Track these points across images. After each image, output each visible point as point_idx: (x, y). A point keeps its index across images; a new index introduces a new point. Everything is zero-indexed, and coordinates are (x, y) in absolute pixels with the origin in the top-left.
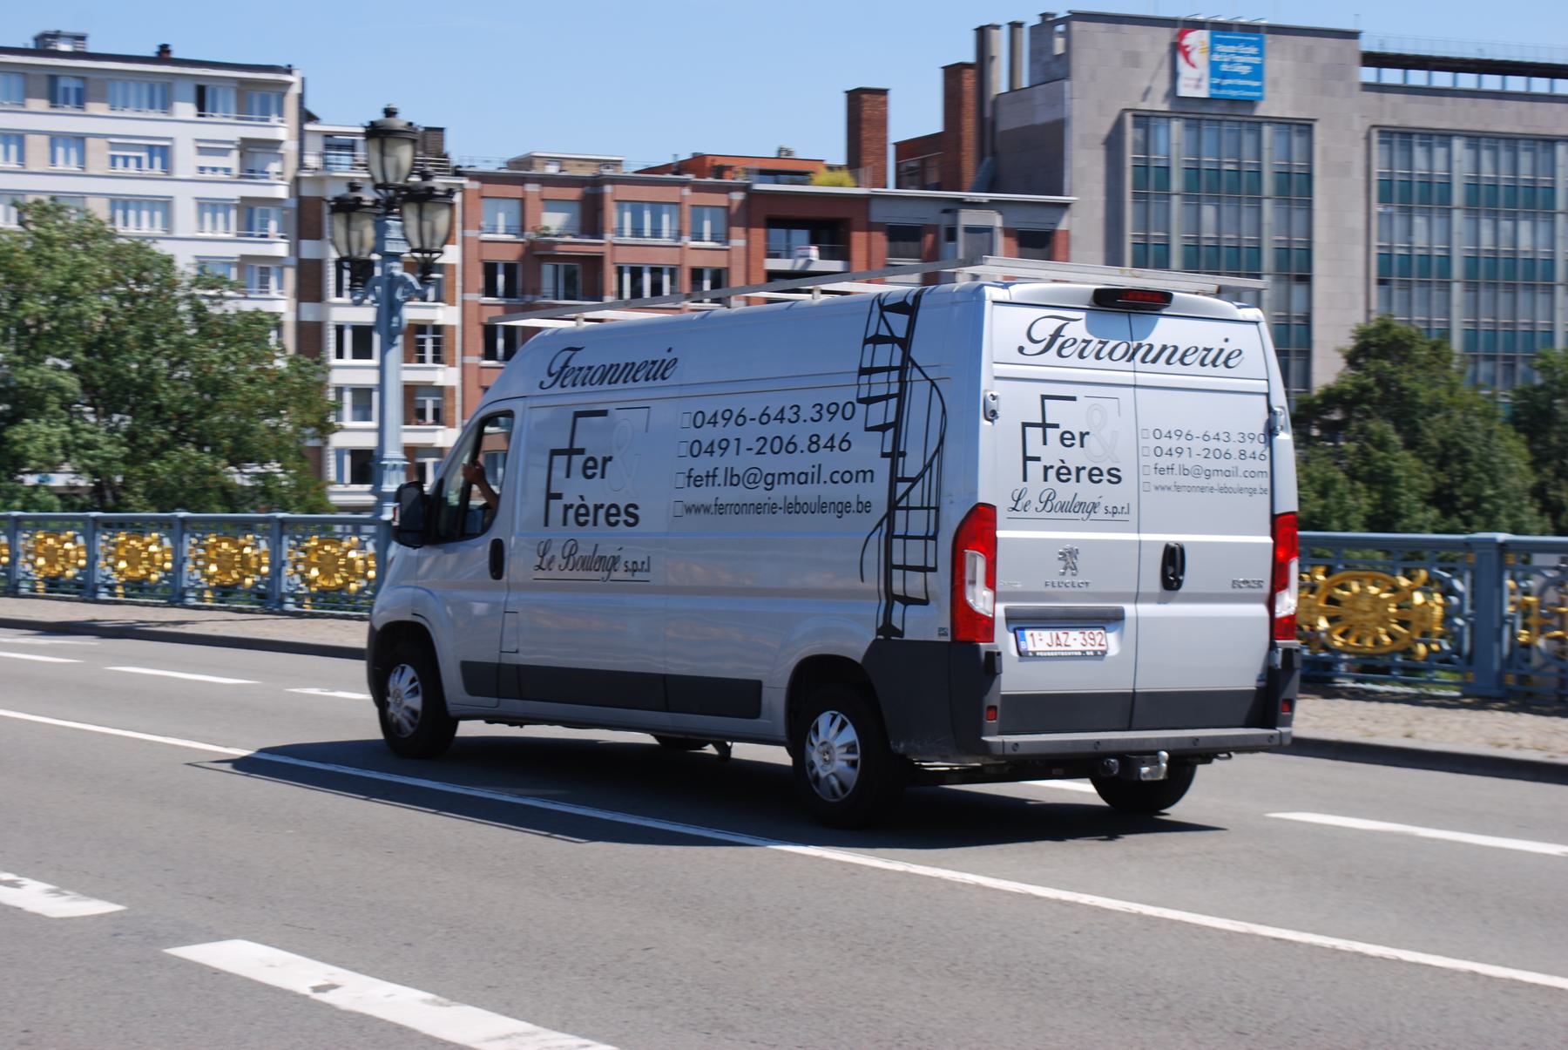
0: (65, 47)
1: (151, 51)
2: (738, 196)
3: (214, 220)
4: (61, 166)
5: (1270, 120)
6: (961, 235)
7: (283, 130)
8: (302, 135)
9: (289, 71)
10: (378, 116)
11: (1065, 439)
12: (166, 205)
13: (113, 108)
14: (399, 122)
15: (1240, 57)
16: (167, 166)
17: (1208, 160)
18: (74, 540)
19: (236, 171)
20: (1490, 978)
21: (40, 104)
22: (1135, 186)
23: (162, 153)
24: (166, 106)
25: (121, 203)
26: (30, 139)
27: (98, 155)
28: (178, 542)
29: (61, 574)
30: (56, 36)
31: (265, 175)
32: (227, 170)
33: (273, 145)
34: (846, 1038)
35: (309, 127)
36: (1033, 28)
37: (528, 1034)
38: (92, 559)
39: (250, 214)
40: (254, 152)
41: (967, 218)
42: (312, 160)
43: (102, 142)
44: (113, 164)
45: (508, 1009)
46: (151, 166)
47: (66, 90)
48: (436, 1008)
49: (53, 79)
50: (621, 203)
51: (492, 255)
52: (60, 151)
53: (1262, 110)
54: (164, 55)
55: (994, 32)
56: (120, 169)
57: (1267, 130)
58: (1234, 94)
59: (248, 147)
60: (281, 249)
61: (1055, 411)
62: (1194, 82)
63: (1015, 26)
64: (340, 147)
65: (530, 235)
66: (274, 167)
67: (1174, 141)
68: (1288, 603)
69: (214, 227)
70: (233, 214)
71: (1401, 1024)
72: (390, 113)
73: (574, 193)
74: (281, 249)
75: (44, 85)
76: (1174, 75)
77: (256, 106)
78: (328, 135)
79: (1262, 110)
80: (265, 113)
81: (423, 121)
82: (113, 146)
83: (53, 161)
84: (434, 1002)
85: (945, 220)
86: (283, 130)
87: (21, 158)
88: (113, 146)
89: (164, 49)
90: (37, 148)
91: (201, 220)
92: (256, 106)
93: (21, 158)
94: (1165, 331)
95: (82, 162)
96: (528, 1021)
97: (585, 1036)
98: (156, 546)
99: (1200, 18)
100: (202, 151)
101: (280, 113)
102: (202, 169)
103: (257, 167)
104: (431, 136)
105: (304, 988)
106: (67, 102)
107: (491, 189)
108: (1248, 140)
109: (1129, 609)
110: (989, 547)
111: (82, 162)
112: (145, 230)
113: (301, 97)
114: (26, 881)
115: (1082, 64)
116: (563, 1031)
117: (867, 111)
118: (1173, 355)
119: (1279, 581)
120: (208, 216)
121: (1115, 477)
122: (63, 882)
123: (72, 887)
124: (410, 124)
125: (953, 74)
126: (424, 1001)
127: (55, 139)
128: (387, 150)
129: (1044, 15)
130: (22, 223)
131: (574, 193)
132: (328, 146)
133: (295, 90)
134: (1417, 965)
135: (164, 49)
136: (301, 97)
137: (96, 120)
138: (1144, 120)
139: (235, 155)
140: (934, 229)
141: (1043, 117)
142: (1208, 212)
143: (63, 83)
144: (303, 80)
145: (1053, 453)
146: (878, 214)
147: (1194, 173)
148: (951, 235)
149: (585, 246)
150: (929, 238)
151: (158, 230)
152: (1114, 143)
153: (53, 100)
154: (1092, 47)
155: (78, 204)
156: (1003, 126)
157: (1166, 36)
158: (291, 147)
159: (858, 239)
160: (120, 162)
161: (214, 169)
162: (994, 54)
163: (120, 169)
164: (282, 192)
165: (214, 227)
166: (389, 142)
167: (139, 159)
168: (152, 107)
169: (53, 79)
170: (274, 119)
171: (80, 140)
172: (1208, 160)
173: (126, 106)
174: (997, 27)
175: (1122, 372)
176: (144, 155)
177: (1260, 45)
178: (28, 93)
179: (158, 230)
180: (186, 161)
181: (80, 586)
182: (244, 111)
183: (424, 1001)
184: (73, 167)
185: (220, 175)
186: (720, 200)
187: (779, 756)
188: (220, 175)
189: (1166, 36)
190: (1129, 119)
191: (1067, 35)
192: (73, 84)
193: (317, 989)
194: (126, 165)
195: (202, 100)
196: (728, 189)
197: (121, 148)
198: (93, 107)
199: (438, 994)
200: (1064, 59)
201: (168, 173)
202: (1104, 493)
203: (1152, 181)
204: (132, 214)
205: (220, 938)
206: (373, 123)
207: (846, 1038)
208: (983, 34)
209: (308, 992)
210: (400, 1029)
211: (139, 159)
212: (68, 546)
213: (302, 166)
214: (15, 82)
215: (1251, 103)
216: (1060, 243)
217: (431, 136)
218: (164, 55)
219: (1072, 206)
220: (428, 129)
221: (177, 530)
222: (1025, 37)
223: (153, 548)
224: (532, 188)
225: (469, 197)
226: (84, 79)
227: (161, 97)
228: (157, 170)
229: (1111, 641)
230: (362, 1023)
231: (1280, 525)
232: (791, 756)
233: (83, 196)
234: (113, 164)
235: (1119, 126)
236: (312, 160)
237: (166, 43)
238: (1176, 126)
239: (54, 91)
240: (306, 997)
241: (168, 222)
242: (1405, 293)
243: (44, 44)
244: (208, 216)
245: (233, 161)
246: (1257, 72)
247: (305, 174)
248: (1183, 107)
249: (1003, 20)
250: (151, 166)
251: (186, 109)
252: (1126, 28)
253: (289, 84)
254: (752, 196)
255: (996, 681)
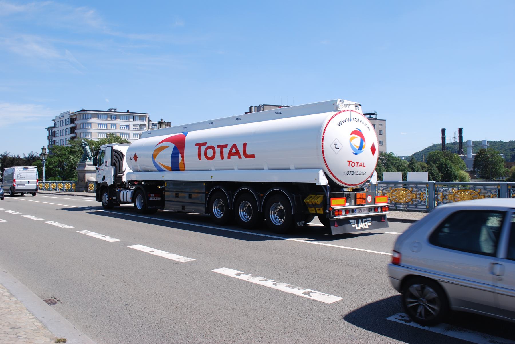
0: (113, 111)
1: (126, 111)
3: (136, 136)
4: (113, 128)
7: (146, 123)
8: (149, 123)
9: (147, 114)
10: (160, 121)
11: (21, 175)
12: (129, 134)
14: (163, 121)
16: (129, 128)
18: (70, 184)
19: (139, 129)
20: (325, 245)
23: (128, 127)
24: (128, 119)
25: (121, 134)
27: (118, 127)
28: (63, 184)
29: (68, 188)
30: (112, 109)
32: (138, 129)
34: (230, 257)
35: (150, 122)
36: (258, 107)
37: (182, 258)
38: (72, 186)
42: (150, 127)
43: (119, 125)
44: (121, 128)
45: (97, 233)
46: (126, 128)
47: (113, 117)
48: (169, 254)
49: (111, 116)
54: (128, 112)
55: (252, 107)
56: (122, 129)
59: (141, 125)
61: (20, 174)
63: (255, 107)
64: (155, 125)
66: (145, 128)
68: (38, 184)
69: (136, 137)
71: (312, 253)
72: (161, 120)
75: (110, 116)
78: (153, 123)
80: (143, 120)
81: (167, 121)
82: (120, 125)
83: (111, 128)
84: (168, 253)
86: (146, 123)
87: (107, 127)
88: (120, 125)
89: (128, 111)
90: (109, 126)
91: (134, 136)
93: (107, 127)
94: (28, 169)
95: (116, 128)
96: (182, 256)
97: (191, 258)
98: (62, 185)
99: (283, 105)
101: (146, 120)
102: (134, 129)
104: (168, 123)
105: (11, 213)
106: (113, 119)
109: (26, 184)
110: (15, 181)
111: (116, 128)
112: (125, 138)
113: (149, 118)
114: (107, 236)
116: (188, 257)
118: (29, 171)
119: (37, 183)
121: (24, 177)
122: (112, 236)
123: (114, 237)
124: (165, 122)
126: (167, 253)
127: (112, 124)
128: (161, 126)
129: (260, 105)
130: (107, 137)
132: (153, 125)
133: (148, 117)
134: (314, 244)
135: (128, 111)
136: (149, 118)
137: (118, 122)
143: (113, 116)
144: (149, 115)
145: (20, 176)
151: (127, 138)
153: (111, 119)
155: (115, 134)
158: (147, 125)
160: (122, 128)
161: (136, 129)
162: (252, 111)
163: (122, 129)
165: (136, 137)
166: (161, 124)
167: (124, 128)
168: (126, 119)
169: (111, 116)
170: (145, 121)
171: (116, 124)
173: (122, 119)
174: (253, 107)
175: (25, 172)
178: (108, 118)
179: (127, 138)
180: (132, 127)
181: (63, 189)
182: (140, 120)
183: (167, 253)
184: (115, 129)
185: (137, 130)
187: (132, 205)
188: (137, 130)
191: (263, 108)
192: (114, 116)
193: (150, 252)
194: (122, 128)
195: (134, 118)
198: (117, 120)
199: (169, 252)
201: (91, 137)
202: (24, 178)
205: (136, 244)
206: (159, 122)
207: (230, 257)
208: (251, 108)
209: (149, 252)
210: (163, 257)
211: (124, 128)
212: (69, 185)
213: (149, 128)
214: (106, 116)
217: (168, 123)
218: (128, 112)
220: (168, 122)
221: (63, 183)
222: (257, 108)
223: (69, 185)
226: (116, 115)
227: (128, 118)
229: (24, 186)
230: (157, 257)
231: (37, 180)
233: (116, 133)
234: (121, 128)
236: (150, 127)
239: (111, 117)
240: (149, 253)
241: (129, 137)
243: (110, 110)
245: (139, 127)
249: (254, 106)
250: (126, 128)
251: (131, 120)
252: (272, 107)
253: (147, 116)
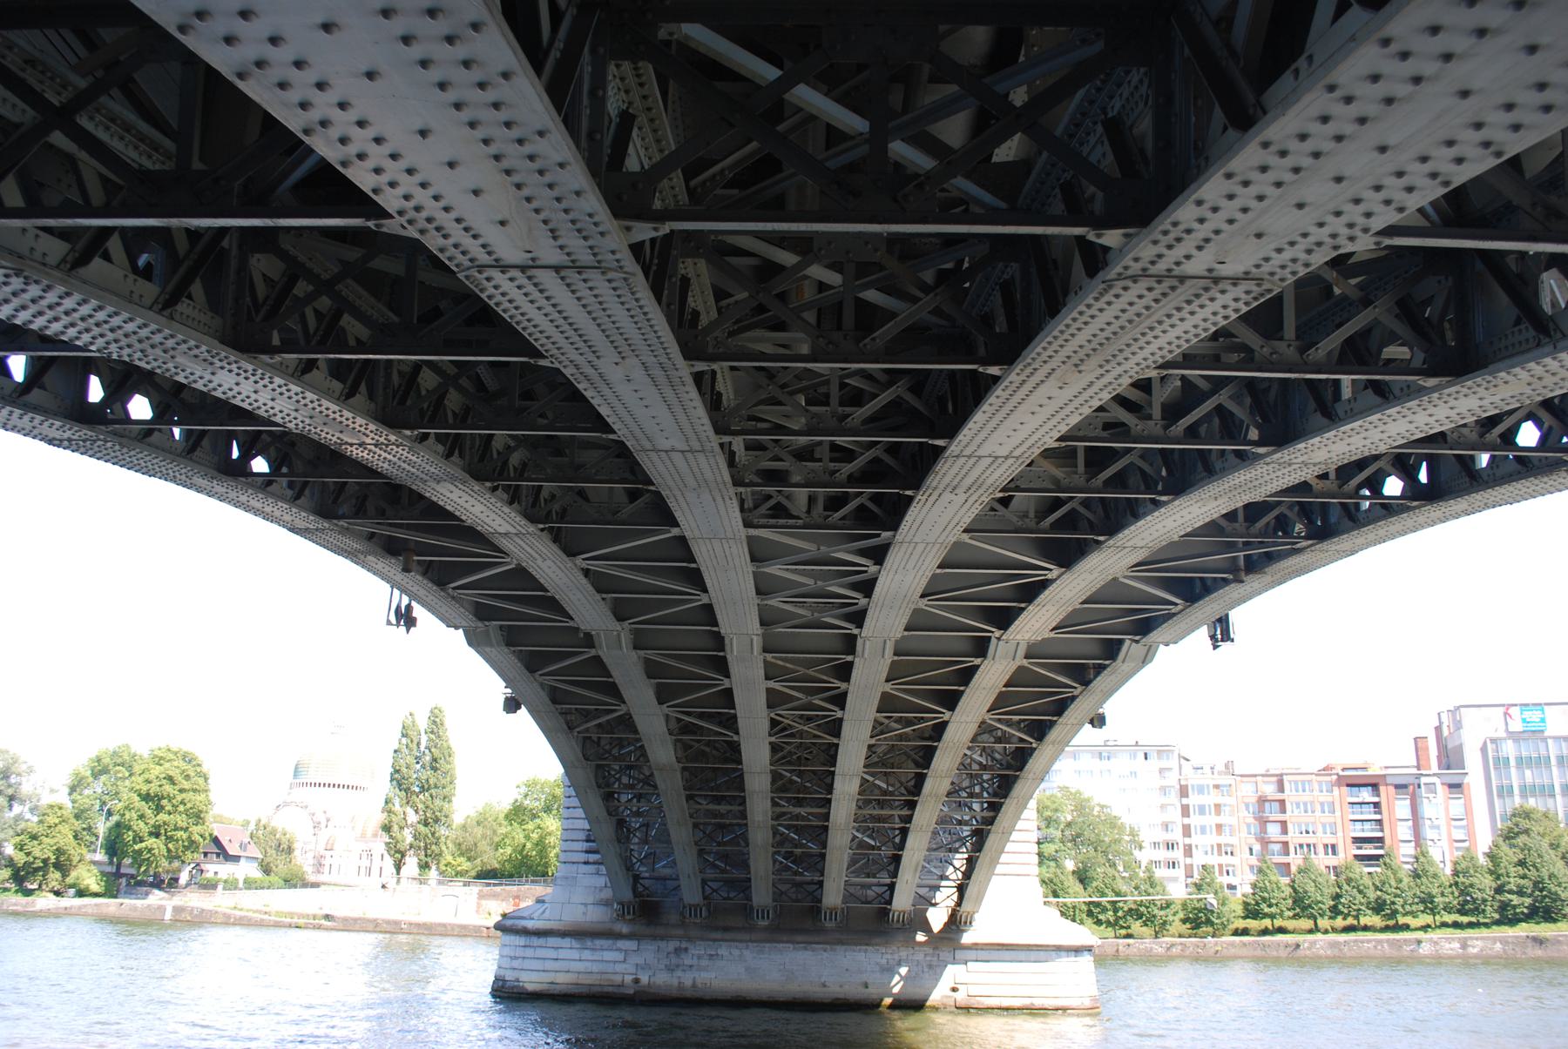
2: (1335, 777)
5: (1550, 737)
6: (1422, 786)
7: (1173, 762)
15: (1535, 716)
17: (1524, 754)
22: (1494, 765)
39: (1164, 790)
41: (1424, 780)
49: (1100, 754)
50: (1290, 782)
51: (1246, 800)
53: (1546, 734)
54: (1137, 744)
57: (1550, 742)
58: (1533, 729)
62: (1516, 726)
65: (1260, 793)
67: (1509, 749)
73: (1275, 779)
76: (1507, 724)
77: (1430, 210)
79: (1546, 734)
85: (1416, 781)
92: (1430, 210)
107: (1245, 779)
108: (1542, 746)
115: (1465, 722)
117: (1420, 745)
125: (1436, 728)
131: (1275, 779)
138: (1493, 741)
140: (1413, 784)
141: (1457, 743)
142: (1528, 773)
146: (1389, 780)
147: (1519, 760)
148: (1419, 786)
149: (1279, 796)
150: (1411, 787)
152: (1484, 750)
154: (1468, 716)
156: (1450, 746)
157: (1502, 709)
159: (1382, 789)
172: (1524, 754)
177: (1543, 710)
186: (1328, 778)
189: (1502, 709)
190: (1488, 742)
196: (1331, 775)
200: (1460, 721)
203: (1502, 763)
215: (1542, 731)
216: (1465, 786)
218: (1137, 744)
224: (1259, 778)
235: (1485, 743)
237: (1108, 720)
238: (1510, 742)
246: (1543, 720)
248: (1512, 735)
254: (1340, 777)
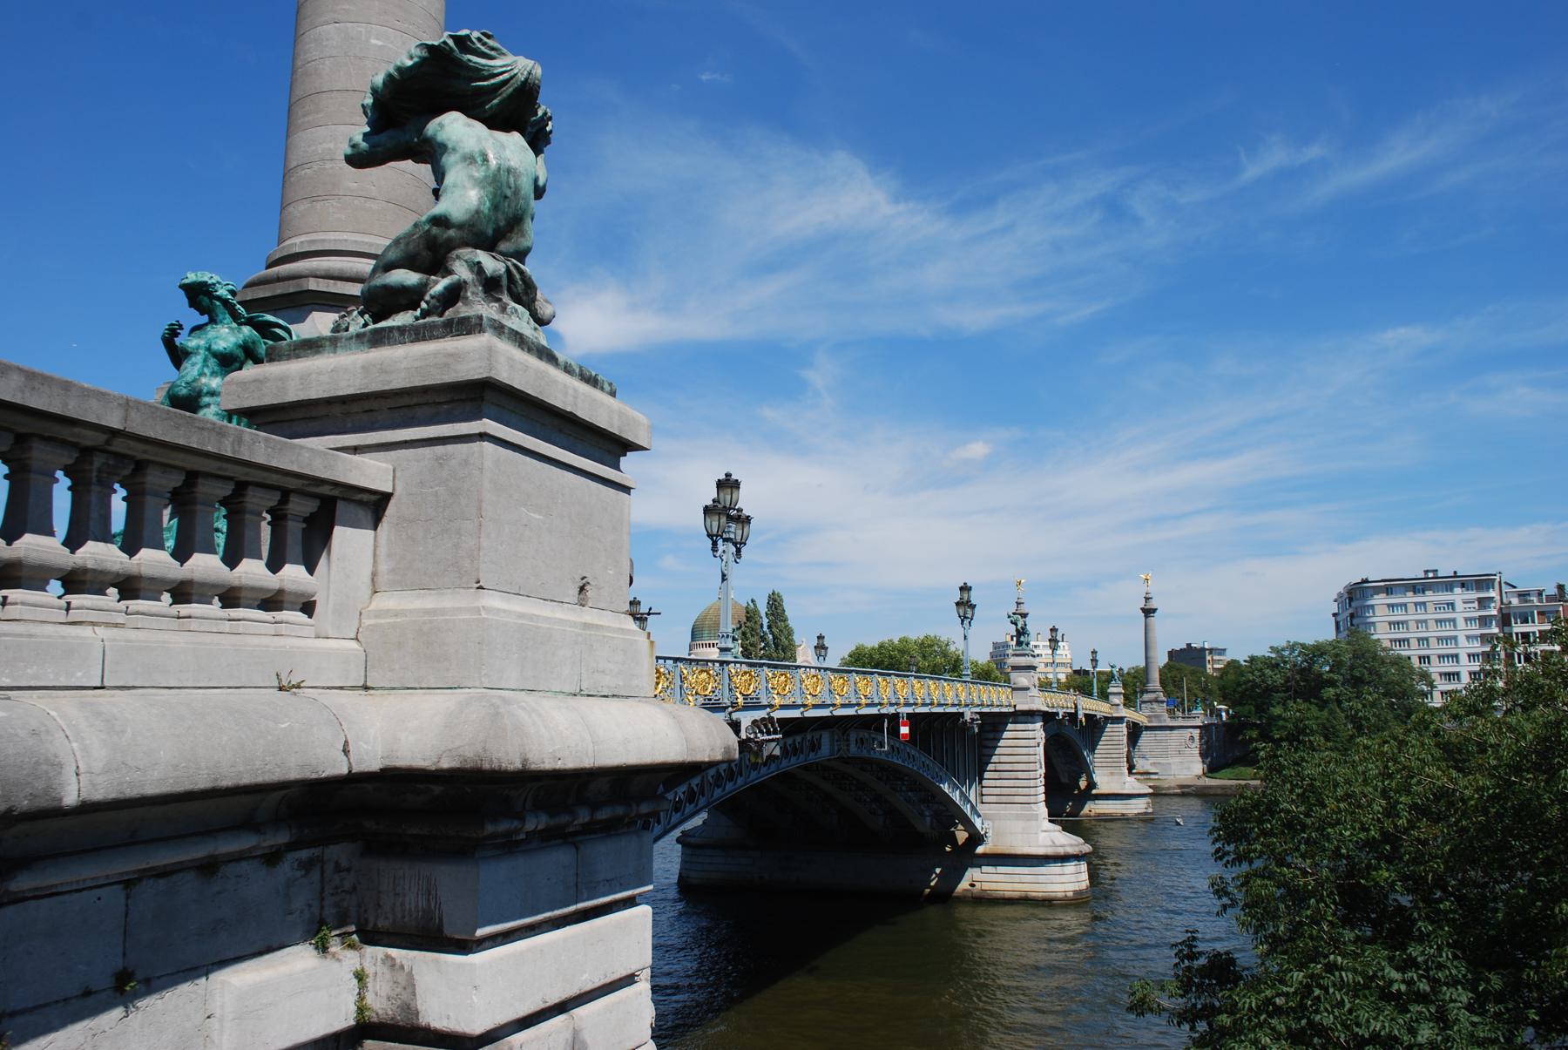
4: (1419, 611)
13: (1434, 592)
19: (1477, 607)
21: (1410, 594)
23: (1452, 605)
24: (1452, 590)
26: (1408, 605)
27: (1430, 607)
31: (1490, 607)
33: (1491, 599)
39: (1484, 621)
40: (1483, 603)
43: (1431, 604)
52: (1418, 607)
59: (1480, 600)
60: (1496, 630)
66: (1493, 605)
69: (1471, 626)
70: (1477, 621)
74: (1496, 630)
80: (1488, 589)
83: (1416, 610)
86: (1493, 593)
91: (1467, 623)
93: (1406, 611)
100: (1464, 603)
103: (1486, 605)
120: (1469, 622)
127: (1416, 604)
133: (1498, 580)
135: (1455, 572)
137: (1429, 597)
139: (1476, 602)
153: (1415, 593)
158: (1498, 598)
163: (1442, 610)
164: (1494, 612)
165: (1471, 626)
168: (1447, 591)
170: (1491, 590)
171: (1424, 603)
176: (1445, 606)
180: (1459, 606)
185: (1472, 609)
192: (1420, 587)
197: (1438, 606)
204: (1447, 624)
213: (1502, 603)
219: (264, 266)
225: (1565, 608)
228: (1451, 610)
232: (283, 566)
242: (200, 480)
244: (1469, 622)
247: (1503, 606)
255: (433, 143)
